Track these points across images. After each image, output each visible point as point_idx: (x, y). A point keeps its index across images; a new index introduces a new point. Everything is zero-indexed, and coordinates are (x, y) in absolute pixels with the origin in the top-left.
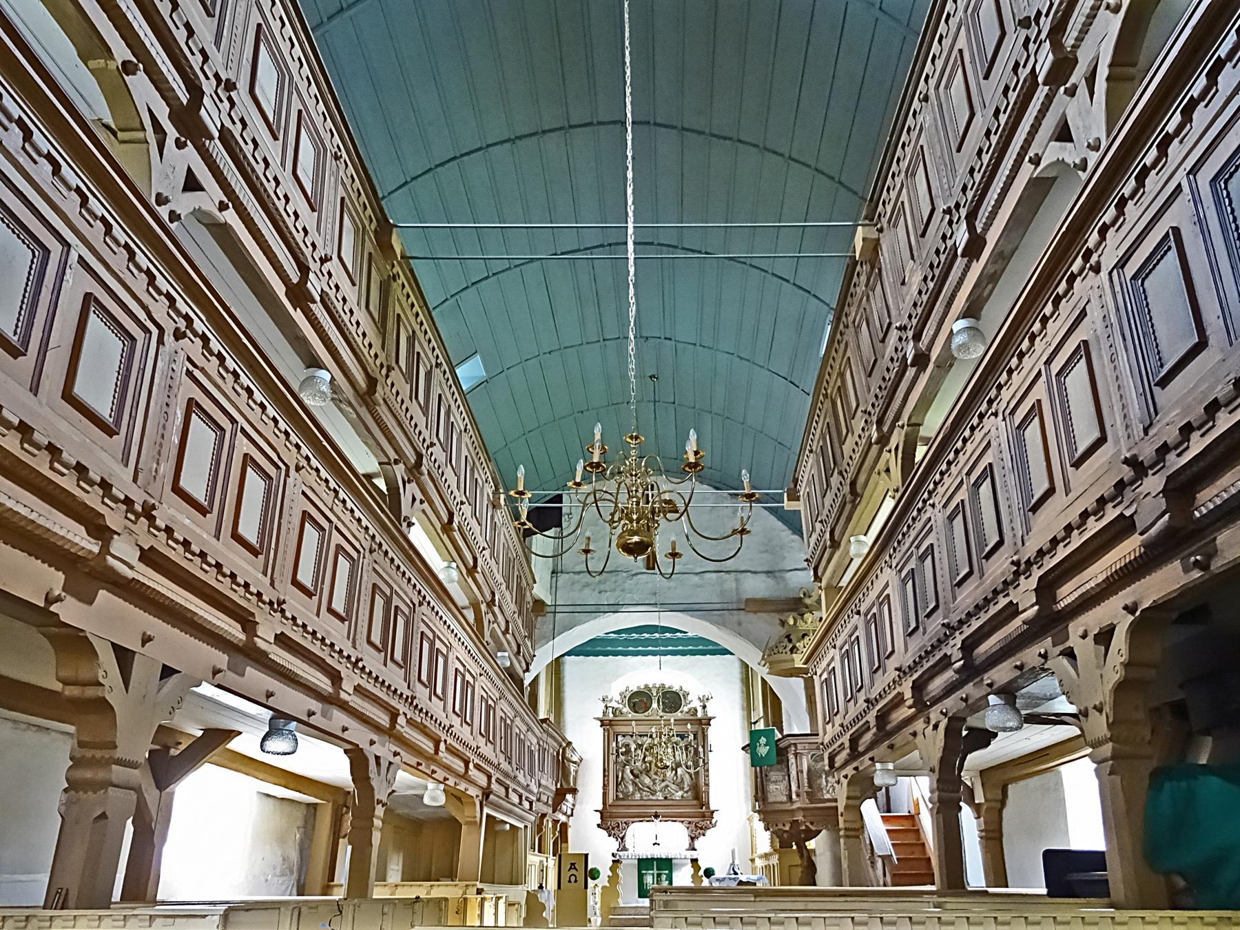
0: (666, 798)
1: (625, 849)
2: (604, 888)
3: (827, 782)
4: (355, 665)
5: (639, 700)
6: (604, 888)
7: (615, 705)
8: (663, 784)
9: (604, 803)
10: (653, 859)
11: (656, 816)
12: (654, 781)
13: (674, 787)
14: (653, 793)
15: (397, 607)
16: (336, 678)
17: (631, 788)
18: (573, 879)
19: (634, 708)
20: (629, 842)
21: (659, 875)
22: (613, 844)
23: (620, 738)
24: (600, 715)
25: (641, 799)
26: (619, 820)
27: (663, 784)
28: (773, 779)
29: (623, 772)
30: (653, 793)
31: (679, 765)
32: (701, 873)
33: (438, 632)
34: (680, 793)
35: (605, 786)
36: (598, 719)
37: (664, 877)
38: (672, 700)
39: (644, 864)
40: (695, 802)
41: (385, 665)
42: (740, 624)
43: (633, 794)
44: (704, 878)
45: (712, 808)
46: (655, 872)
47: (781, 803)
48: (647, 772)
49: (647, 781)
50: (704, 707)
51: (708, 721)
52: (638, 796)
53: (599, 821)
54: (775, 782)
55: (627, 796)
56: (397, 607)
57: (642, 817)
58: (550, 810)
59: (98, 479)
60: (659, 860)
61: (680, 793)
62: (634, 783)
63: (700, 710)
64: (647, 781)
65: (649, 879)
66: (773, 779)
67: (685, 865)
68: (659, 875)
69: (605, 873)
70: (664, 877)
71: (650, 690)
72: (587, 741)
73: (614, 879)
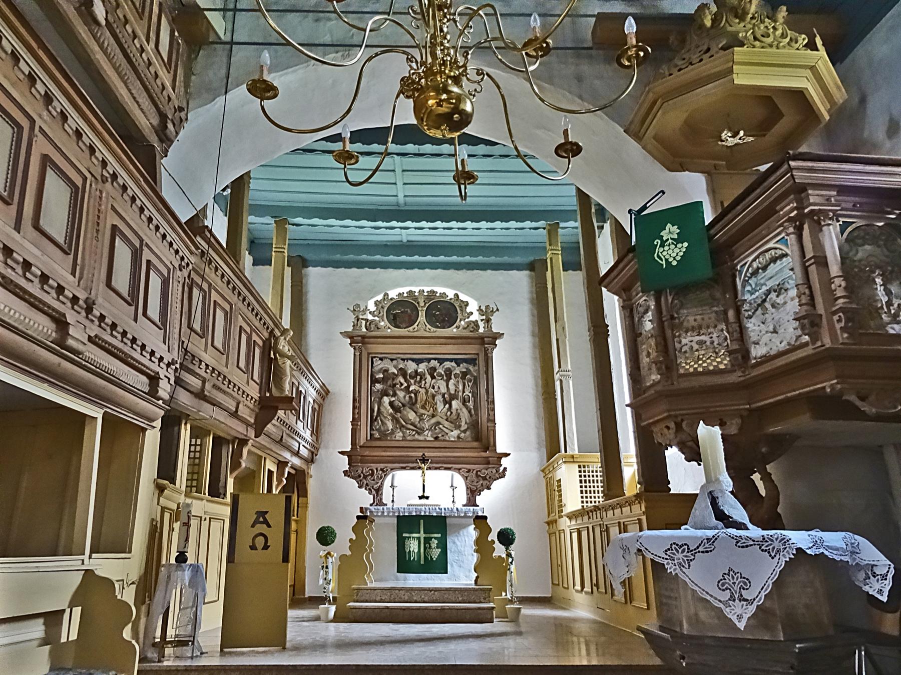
0: (436, 438)
1: (381, 503)
2: (342, 557)
3: (888, 293)
4: (89, 310)
5: (401, 312)
6: (342, 557)
7: (370, 317)
8: (433, 421)
9: (354, 443)
10: (419, 517)
11: (424, 460)
12: (421, 416)
13: (446, 424)
14: (420, 431)
15: (148, 262)
16: (61, 324)
17: (390, 425)
18: (260, 541)
19: (395, 321)
20: (386, 497)
21: (427, 540)
22: (365, 498)
23: (377, 362)
24: (350, 329)
25: (404, 439)
26: (374, 466)
27: (433, 421)
28: (691, 321)
29: (380, 404)
30: (420, 431)
31: (453, 397)
32: (493, 536)
33: (146, 240)
34: (456, 433)
35: (355, 421)
36: (346, 334)
37: (434, 543)
38: (444, 312)
39: (407, 523)
40: (475, 444)
41: (136, 320)
42: (579, 79)
43: (393, 432)
44: (498, 546)
45: (500, 449)
46: (422, 535)
47: (717, 372)
48: (412, 404)
49: (412, 416)
50: (488, 321)
51: (493, 339)
52: (399, 435)
53: (347, 468)
54: (698, 329)
55: (384, 435)
56: (148, 262)
57: (407, 464)
58: (252, 433)
59: (110, 323)
60: (428, 519)
61: (456, 433)
62: (395, 420)
63: (481, 324)
64: (412, 416)
65: (413, 546)
66: (691, 321)
67: (466, 526)
68: (427, 540)
69: (345, 535)
70: (434, 543)
71: (416, 299)
72: (333, 366)
73: (359, 545)
